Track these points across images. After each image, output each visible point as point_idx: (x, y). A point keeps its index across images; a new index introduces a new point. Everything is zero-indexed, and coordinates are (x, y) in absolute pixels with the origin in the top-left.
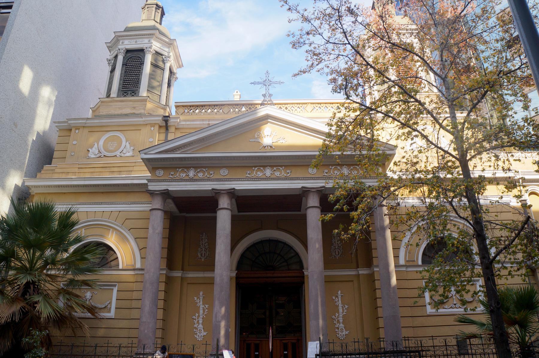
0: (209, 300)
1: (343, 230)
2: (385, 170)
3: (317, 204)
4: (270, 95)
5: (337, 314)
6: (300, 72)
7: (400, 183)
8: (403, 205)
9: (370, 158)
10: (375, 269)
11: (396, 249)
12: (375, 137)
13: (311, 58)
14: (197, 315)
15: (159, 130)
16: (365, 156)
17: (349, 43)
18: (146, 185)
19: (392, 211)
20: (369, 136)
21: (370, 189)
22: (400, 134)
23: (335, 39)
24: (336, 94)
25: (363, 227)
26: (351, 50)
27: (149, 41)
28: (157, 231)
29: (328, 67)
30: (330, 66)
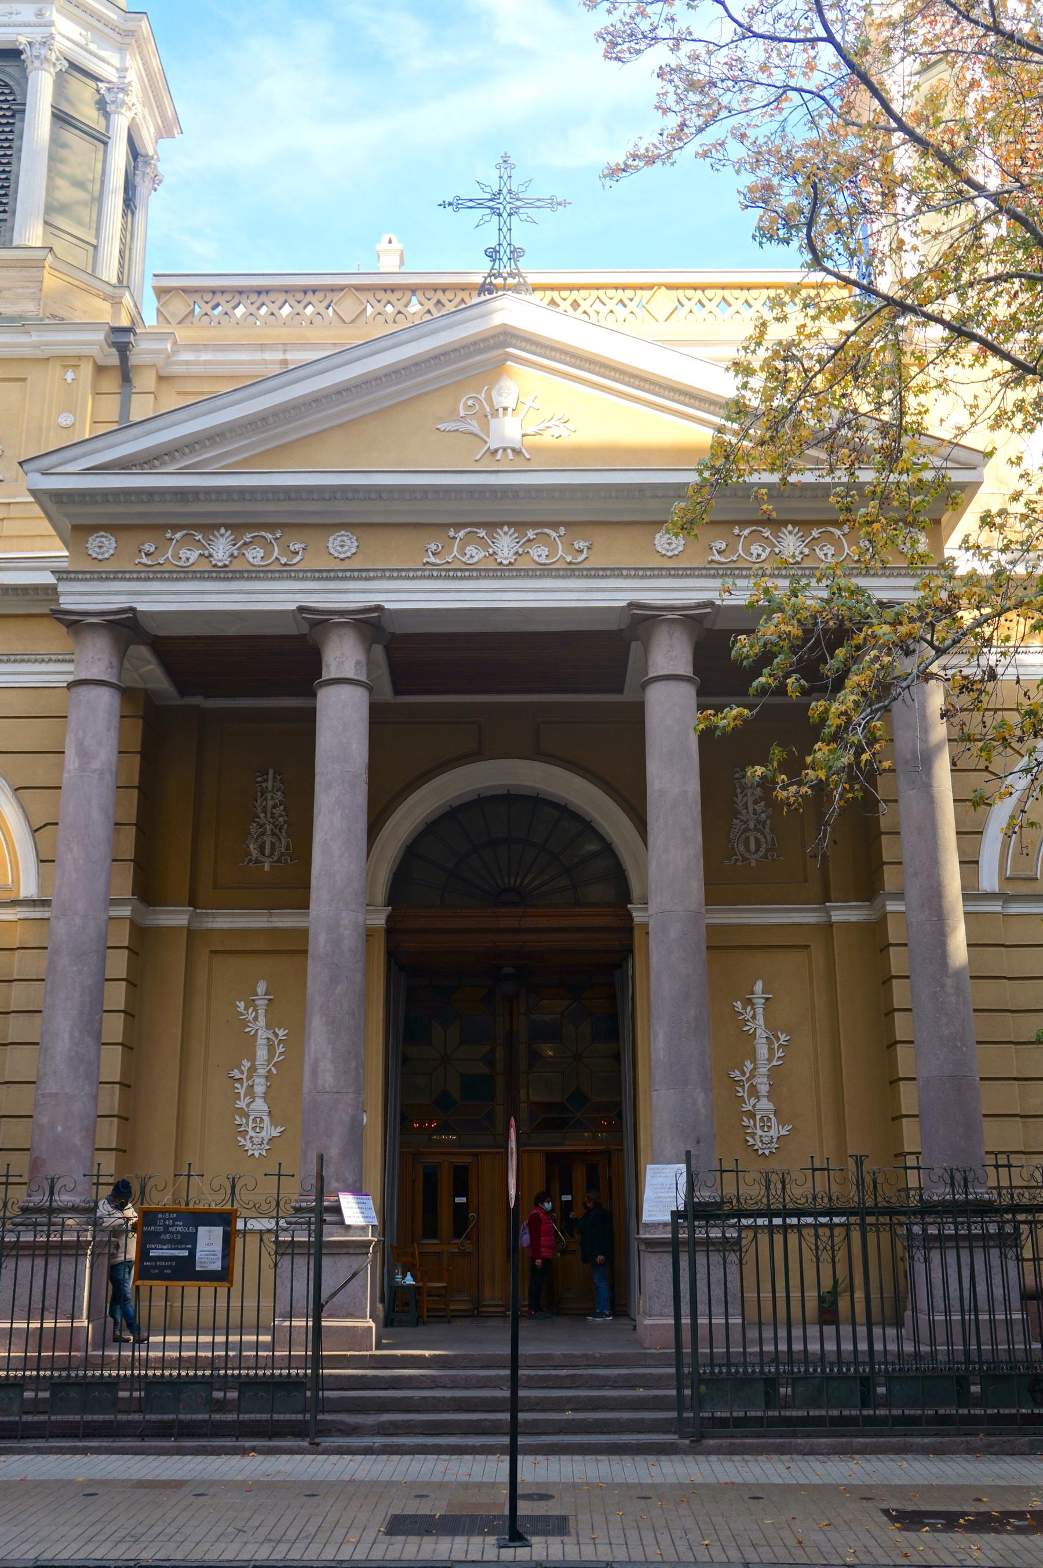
0: (289, 1009)
1: (783, 767)
2: (938, 543)
3: (685, 667)
4: (516, 254)
5: (749, 1066)
6: (635, 157)
7: (1000, 592)
8: (1007, 674)
9: (885, 499)
10: (892, 906)
11: (970, 834)
12: (908, 419)
13: (679, 100)
14: (246, 1064)
15: (95, 383)
16: (868, 489)
17: (830, 39)
18: (49, 592)
19: (966, 699)
20: (887, 415)
21: (889, 614)
22: (1009, 408)
23: (776, 20)
24: (772, 249)
25: (858, 755)
26: (836, 66)
27: (40, 14)
28: (96, 765)
29: (743, 136)
30: (751, 133)
